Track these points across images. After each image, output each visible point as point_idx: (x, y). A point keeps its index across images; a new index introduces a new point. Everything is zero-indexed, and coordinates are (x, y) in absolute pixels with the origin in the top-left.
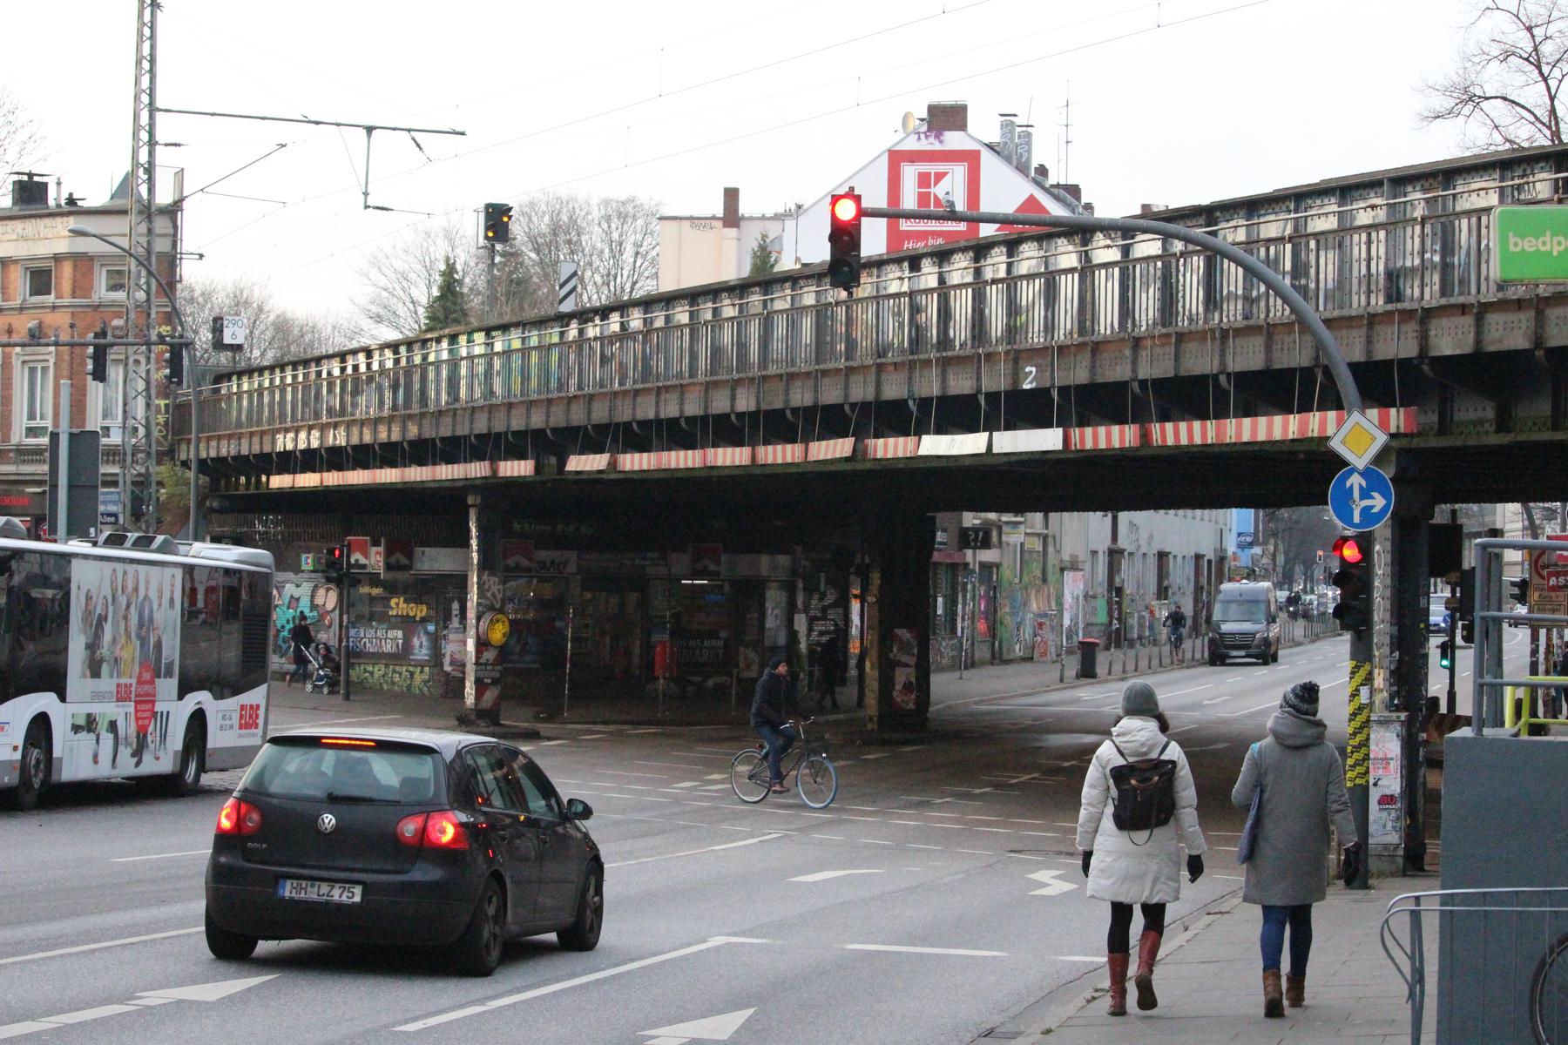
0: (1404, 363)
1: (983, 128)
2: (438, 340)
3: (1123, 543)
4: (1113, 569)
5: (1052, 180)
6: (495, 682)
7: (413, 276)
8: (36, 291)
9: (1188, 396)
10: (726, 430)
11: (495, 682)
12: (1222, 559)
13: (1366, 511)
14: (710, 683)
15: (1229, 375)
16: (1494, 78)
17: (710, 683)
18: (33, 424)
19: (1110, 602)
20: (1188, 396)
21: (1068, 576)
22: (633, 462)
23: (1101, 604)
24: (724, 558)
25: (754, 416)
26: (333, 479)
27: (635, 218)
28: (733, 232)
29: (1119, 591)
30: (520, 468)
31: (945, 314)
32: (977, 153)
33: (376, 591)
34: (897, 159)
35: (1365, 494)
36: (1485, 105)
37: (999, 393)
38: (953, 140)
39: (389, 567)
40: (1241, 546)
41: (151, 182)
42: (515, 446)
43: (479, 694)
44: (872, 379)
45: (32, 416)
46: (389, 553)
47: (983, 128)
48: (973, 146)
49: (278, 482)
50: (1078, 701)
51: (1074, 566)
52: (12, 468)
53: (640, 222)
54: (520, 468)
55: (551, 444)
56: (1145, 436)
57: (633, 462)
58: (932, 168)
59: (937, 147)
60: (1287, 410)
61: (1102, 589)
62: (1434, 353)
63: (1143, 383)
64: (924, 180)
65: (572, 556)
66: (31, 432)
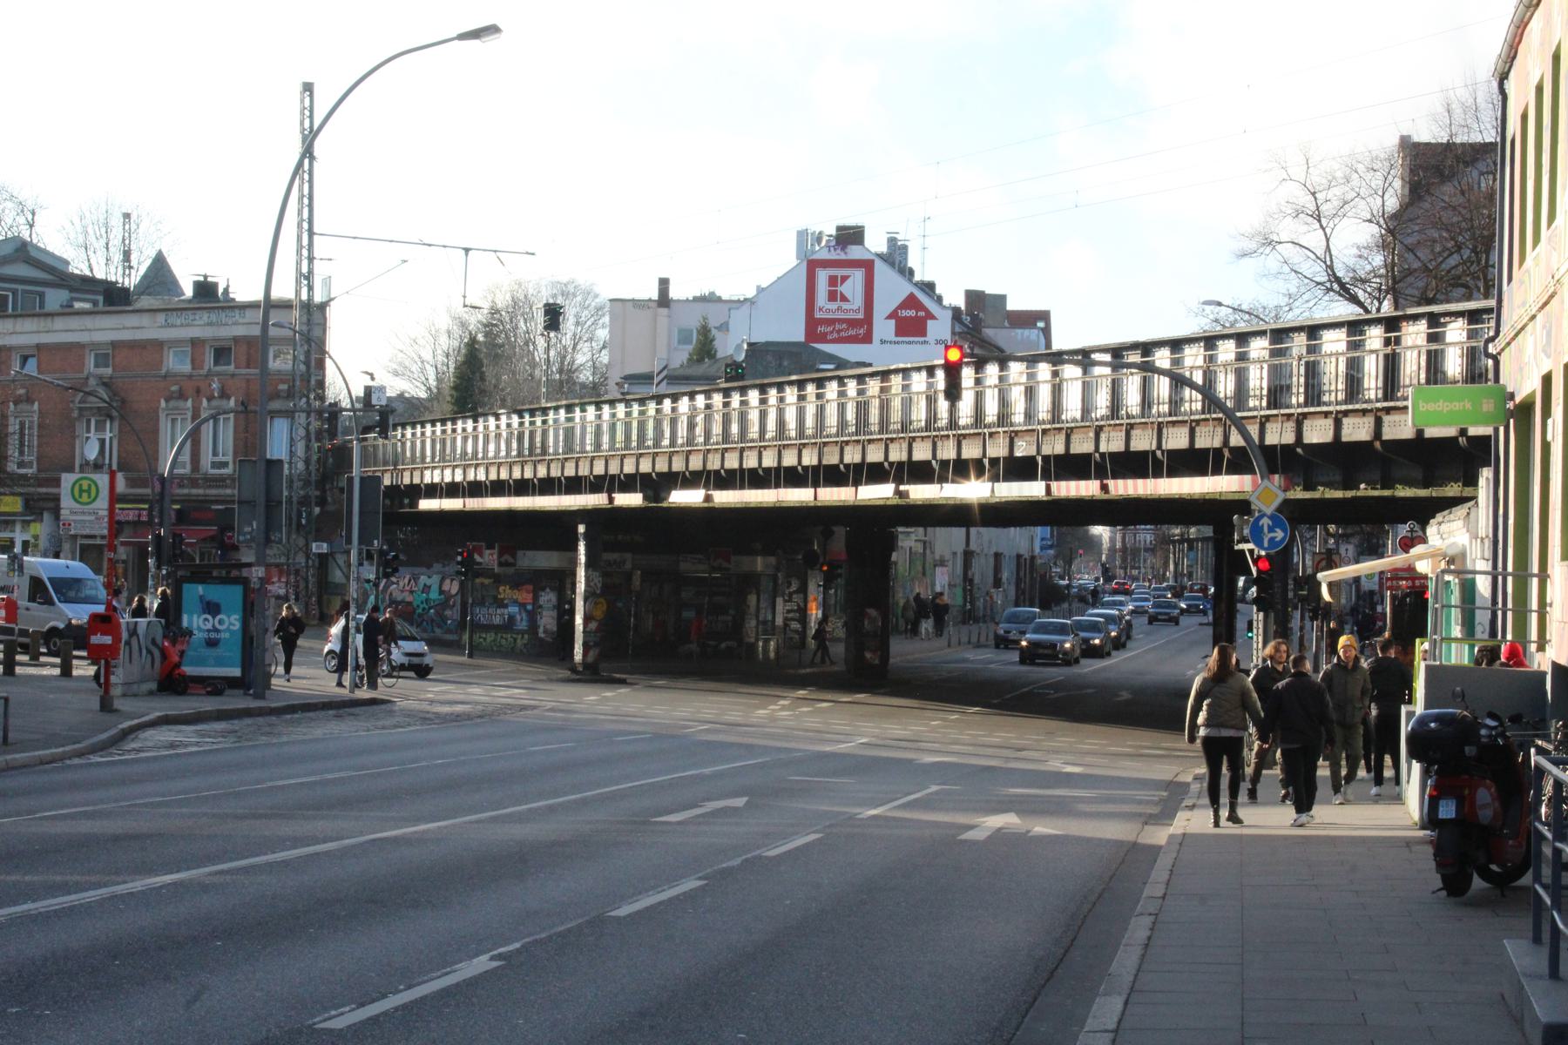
0: (1285, 447)
1: (875, 243)
2: (556, 409)
3: (973, 546)
4: (967, 565)
5: (917, 278)
6: (596, 644)
7: (421, 341)
8: (216, 363)
9: (1133, 464)
10: (794, 477)
11: (596, 644)
12: (1033, 558)
13: (1272, 540)
14: (723, 645)
16: (1287, 229)
17: (723, 645)
18: (216, 459)
19: (964, 590)
20: (1133, 464)
21: (939, 570)
22: (725, 498)
23: (959, 591)
24: (733, 558)
25: (816, 469)
26: (474, 504)
27: (575, 295)
28: (664, 311)
29: (971, 581)
30: (633, 499)
32: (872, 262)
33: (487, 581)
34: (813, 266)
35: (1271, 530)
36: (1279, 247)
38: (854, 252)
39: (501, 564)
40: (1042, 548)
41: (310, 288)
43: (585, 654)
44: (905, 446)
45: (215, 454)
46: (500, 555)
47: (875, 243)
48: (867, 256)
49: (426, 504)
50: (965, 660)
51: (942, 563)
52: (201, 491)
53: (579, 298)
54: (633, 499)
55: (656, 485)
56: (1104, 488)
57: (725, 498)
58: (839, 272)
59: (843, 257)
61: (959, 580)
62: (1306, 441)
63: (1103, 455)
64: (833, 281)
65: (628, 556)
66: (215, 465)
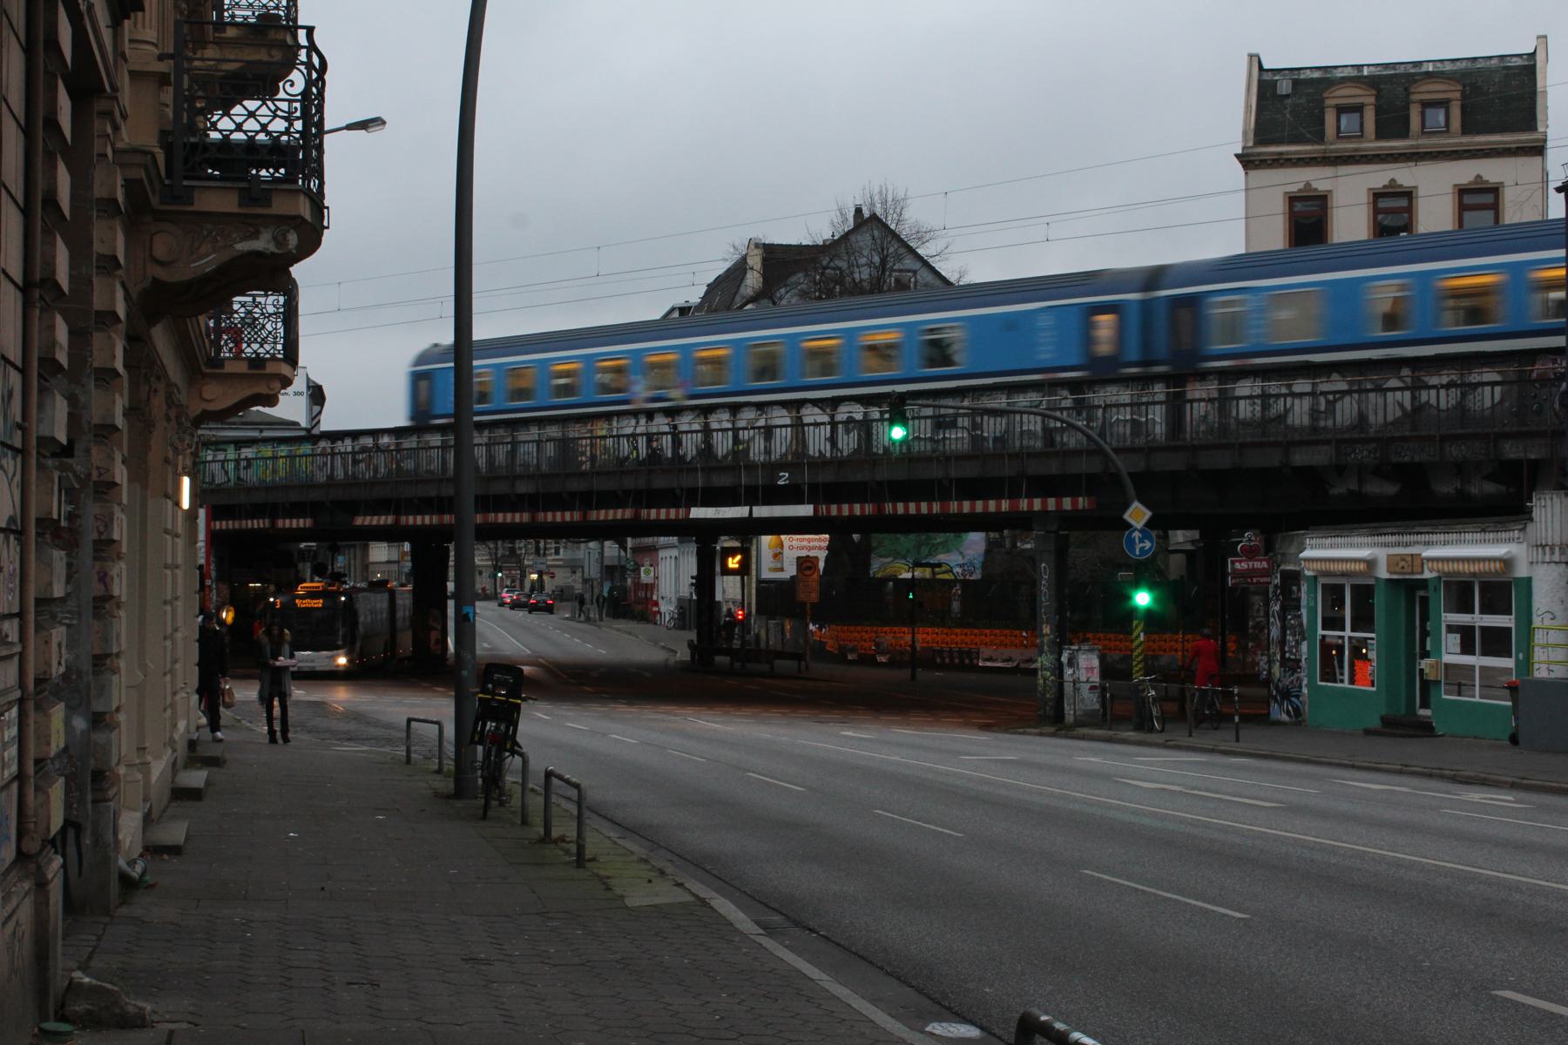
13: (1142, 549)
15: (951, 481)
31: (677, 443)
35: (1141, 541)
37: (756, 488)
42: (295, 510)
60: (234, 519)
